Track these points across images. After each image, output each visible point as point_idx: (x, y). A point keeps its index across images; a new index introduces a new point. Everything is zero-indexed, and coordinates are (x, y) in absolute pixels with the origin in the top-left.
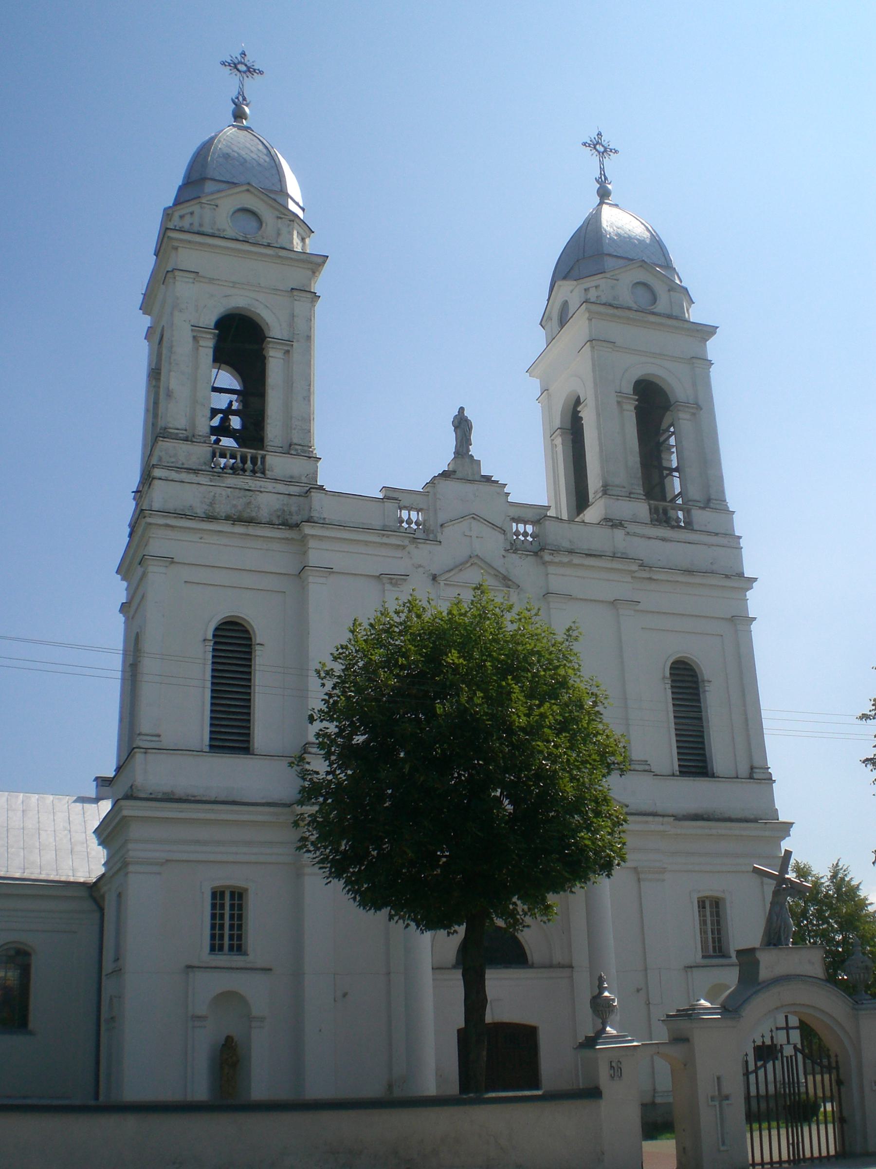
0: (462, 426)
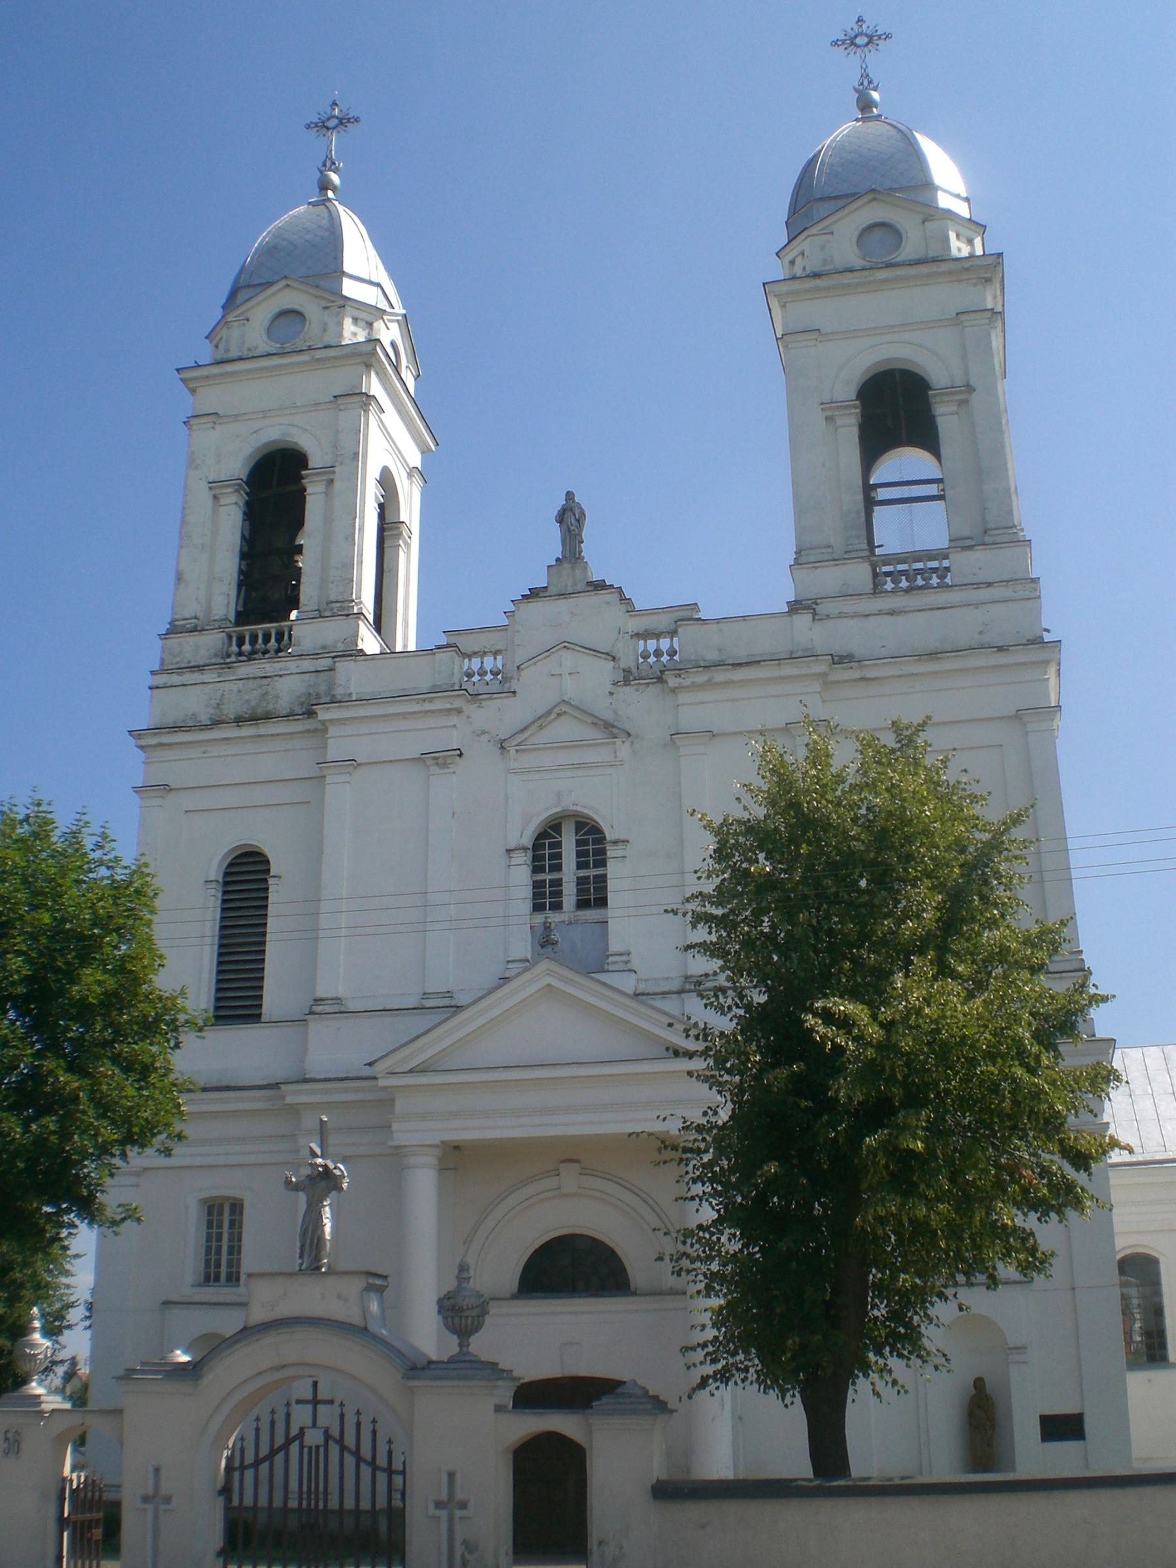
0: (570, 518)
